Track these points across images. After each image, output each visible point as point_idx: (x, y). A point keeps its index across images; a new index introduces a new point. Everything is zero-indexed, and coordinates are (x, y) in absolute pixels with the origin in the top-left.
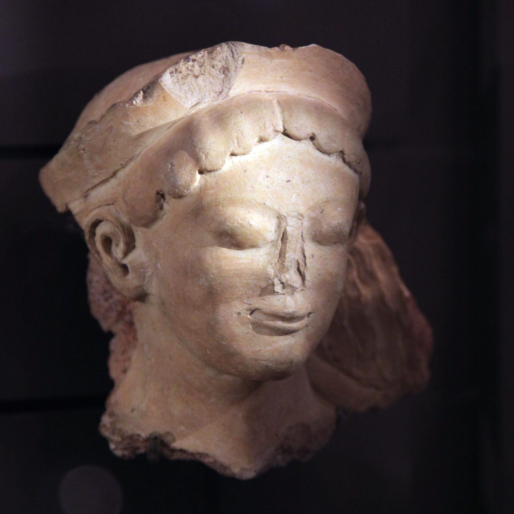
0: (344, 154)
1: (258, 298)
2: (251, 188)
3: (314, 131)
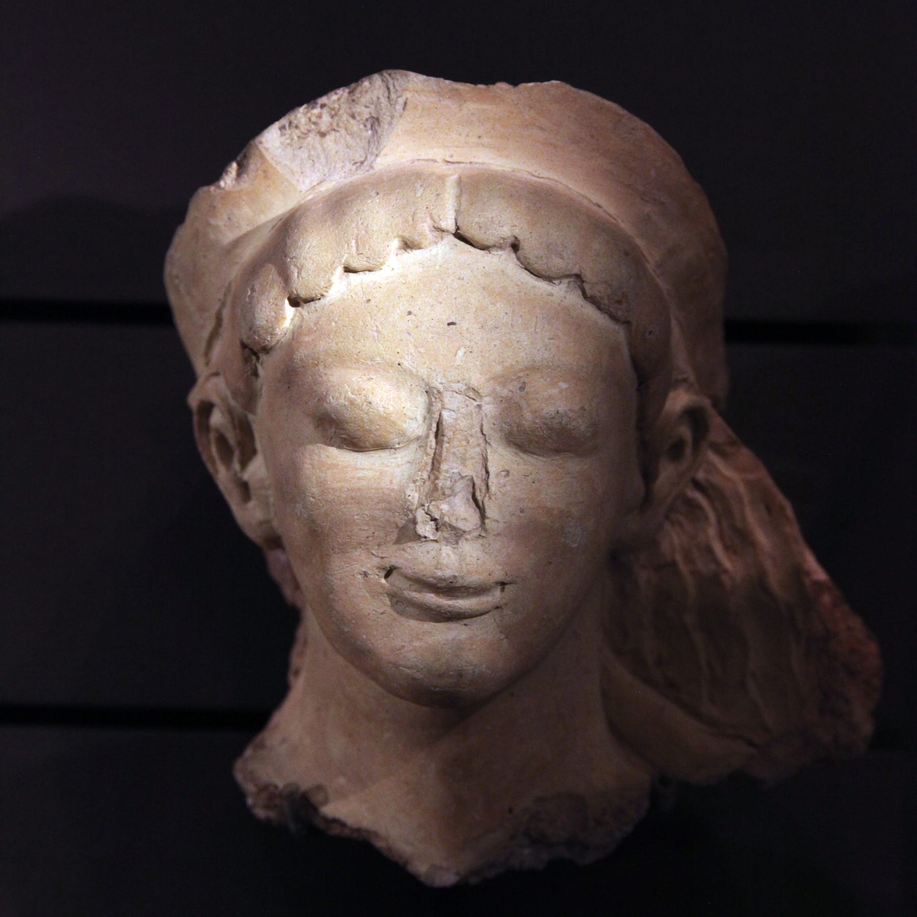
0: (583, 282)
1: (396, 547)
2: (376, 334)
3: (517, 232)
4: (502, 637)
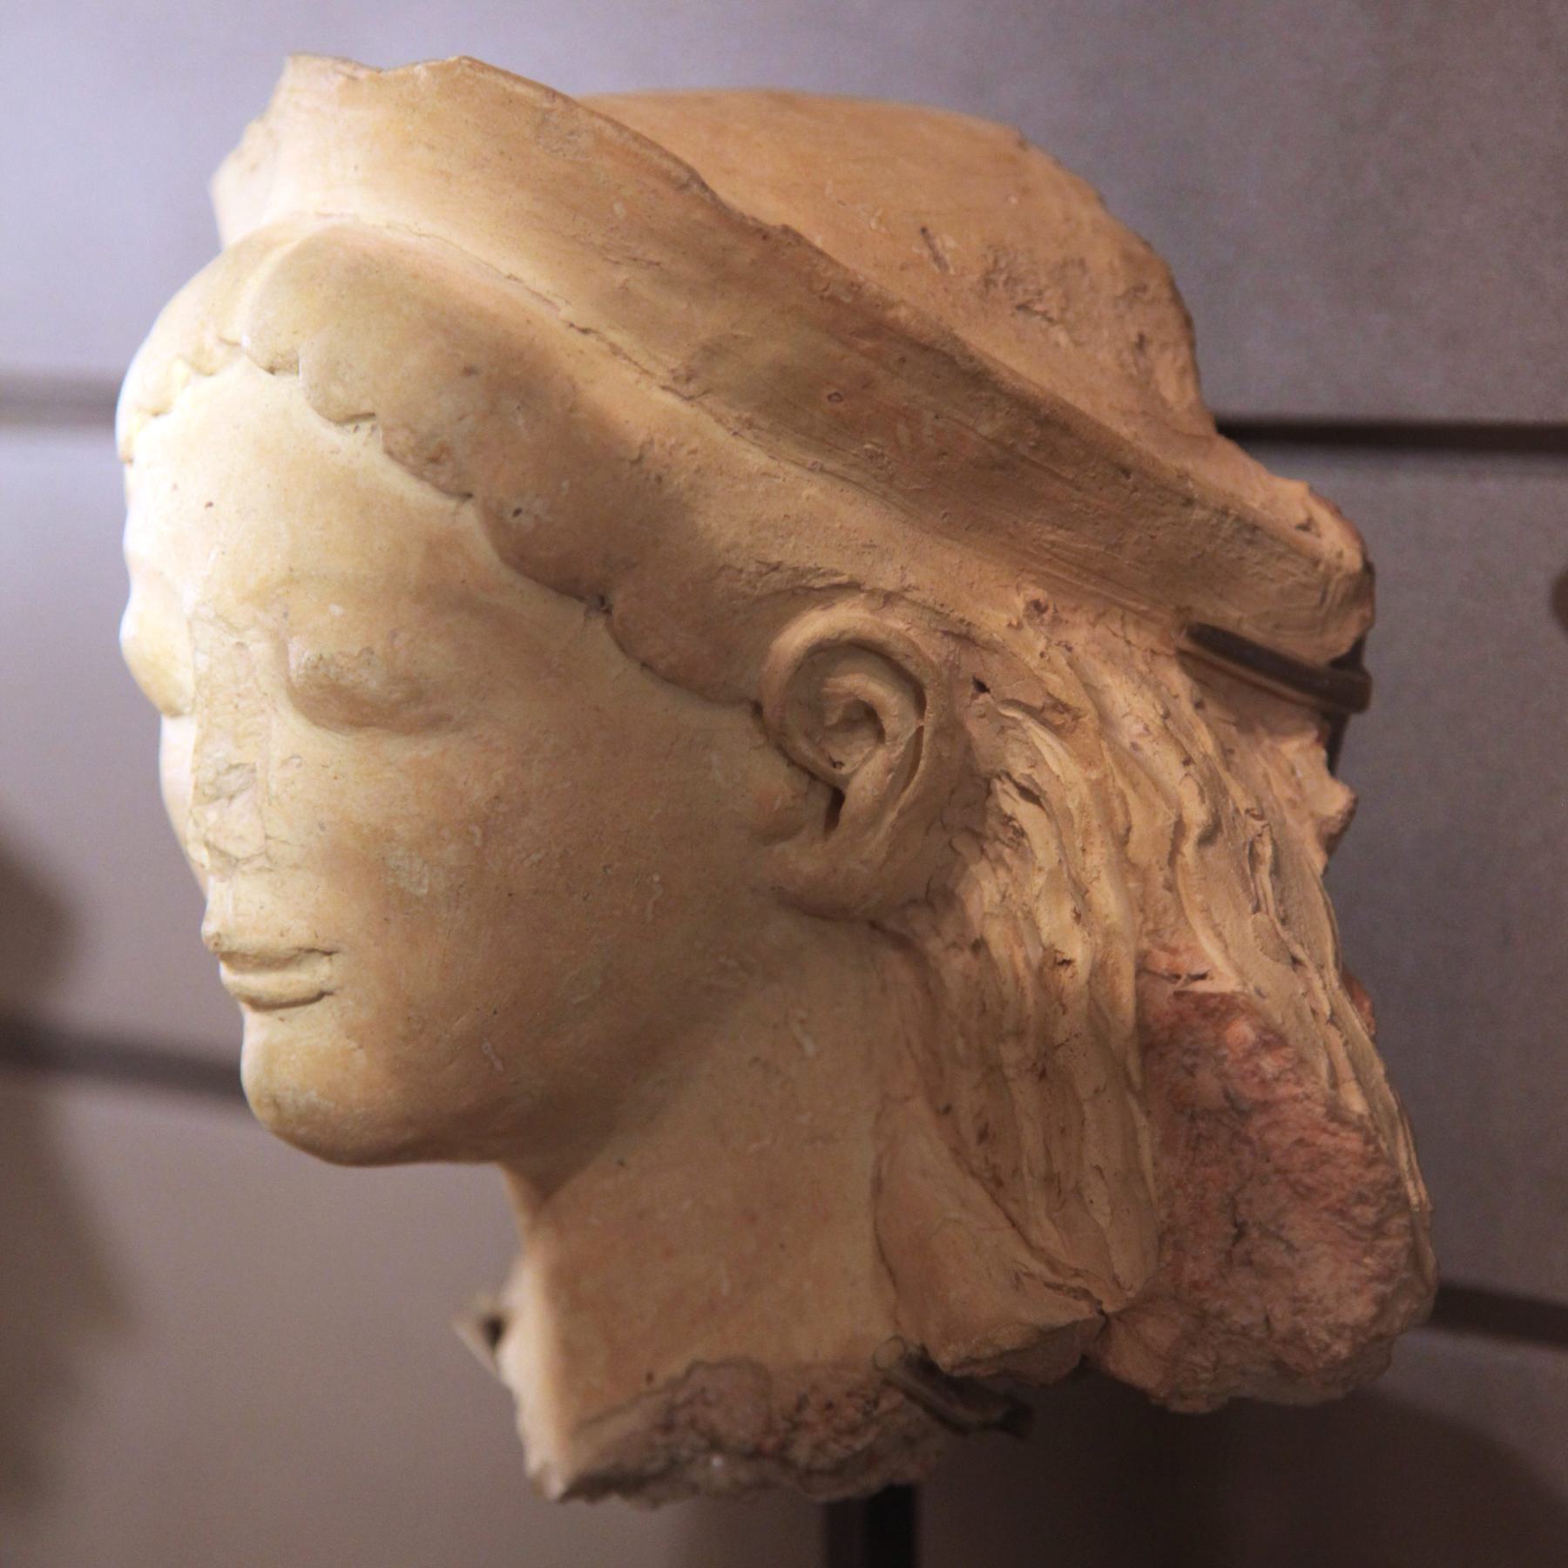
4: (353, 1045)
